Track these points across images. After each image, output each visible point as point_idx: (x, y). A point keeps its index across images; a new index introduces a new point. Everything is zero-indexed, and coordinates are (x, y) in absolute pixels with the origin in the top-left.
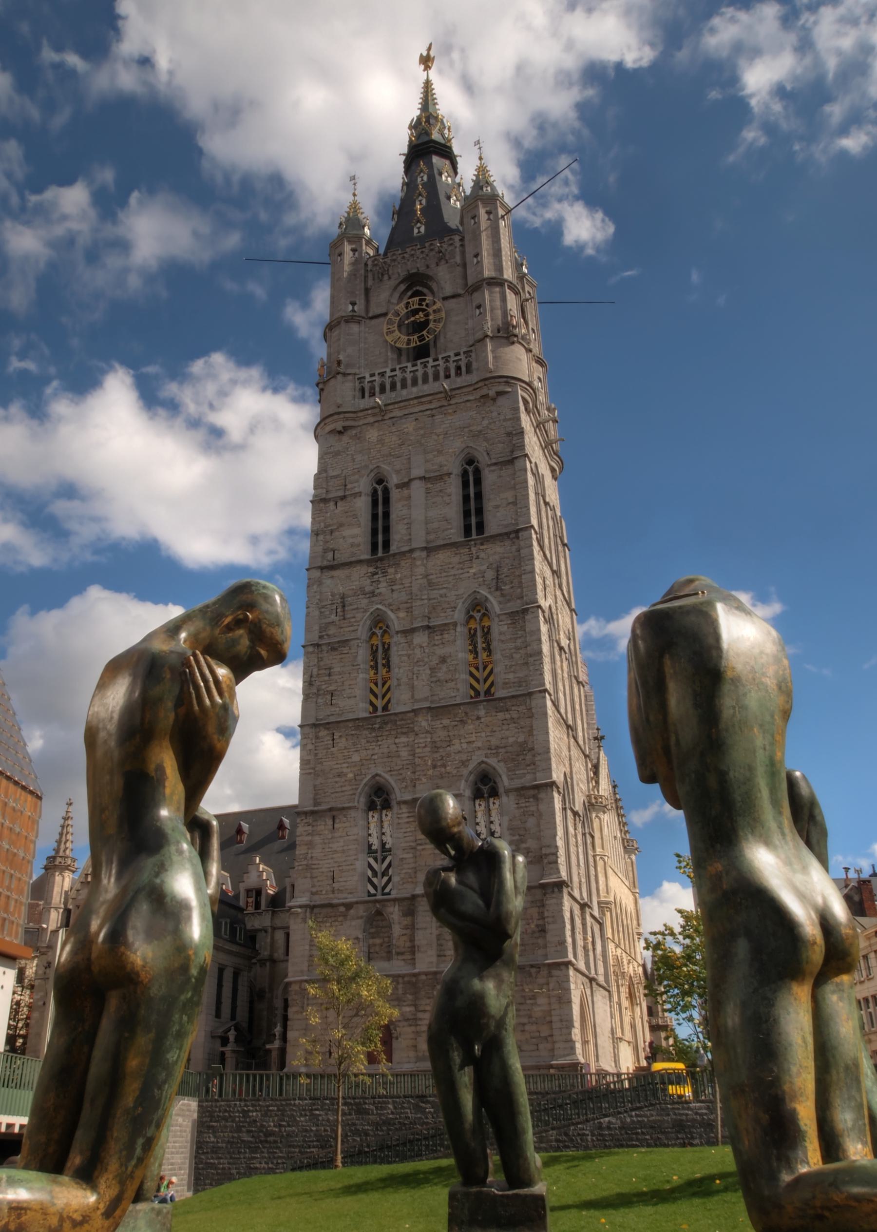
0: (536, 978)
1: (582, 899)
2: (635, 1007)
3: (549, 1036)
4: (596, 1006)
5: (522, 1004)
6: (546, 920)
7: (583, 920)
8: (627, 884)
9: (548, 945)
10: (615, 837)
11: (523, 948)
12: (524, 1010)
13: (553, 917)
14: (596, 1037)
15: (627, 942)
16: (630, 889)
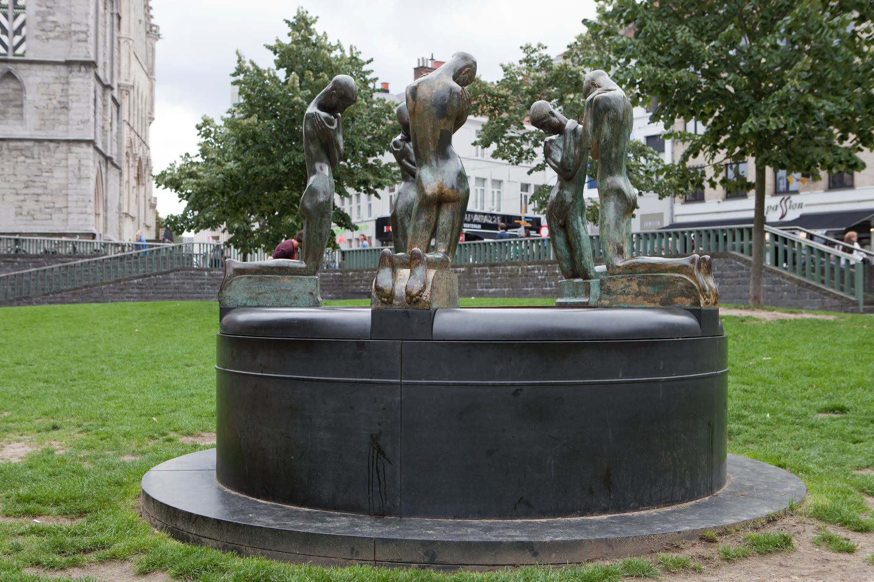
0: (54, 152)
1: (106, 80)
2: (141, 186)
3: (64, 207)
4: (109, 182)
5: (39, 176)
6: (70, 98)
7: (104, 100)
8: (146, 68)
9: (70, 122)
10: (140, 21)
11: (43, 122)
12: (40, 182)
13: (78, 95)
14: (106, 211)
15: (140, 126)
16: (147, 74)
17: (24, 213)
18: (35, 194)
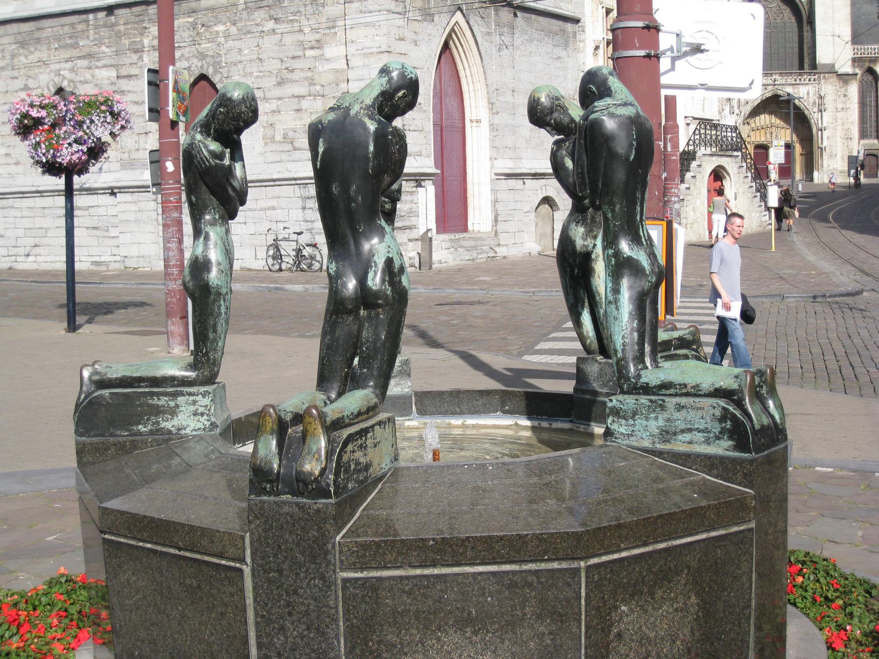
5: (298, 57)
17: (278, 138)
18: (294, 96)
